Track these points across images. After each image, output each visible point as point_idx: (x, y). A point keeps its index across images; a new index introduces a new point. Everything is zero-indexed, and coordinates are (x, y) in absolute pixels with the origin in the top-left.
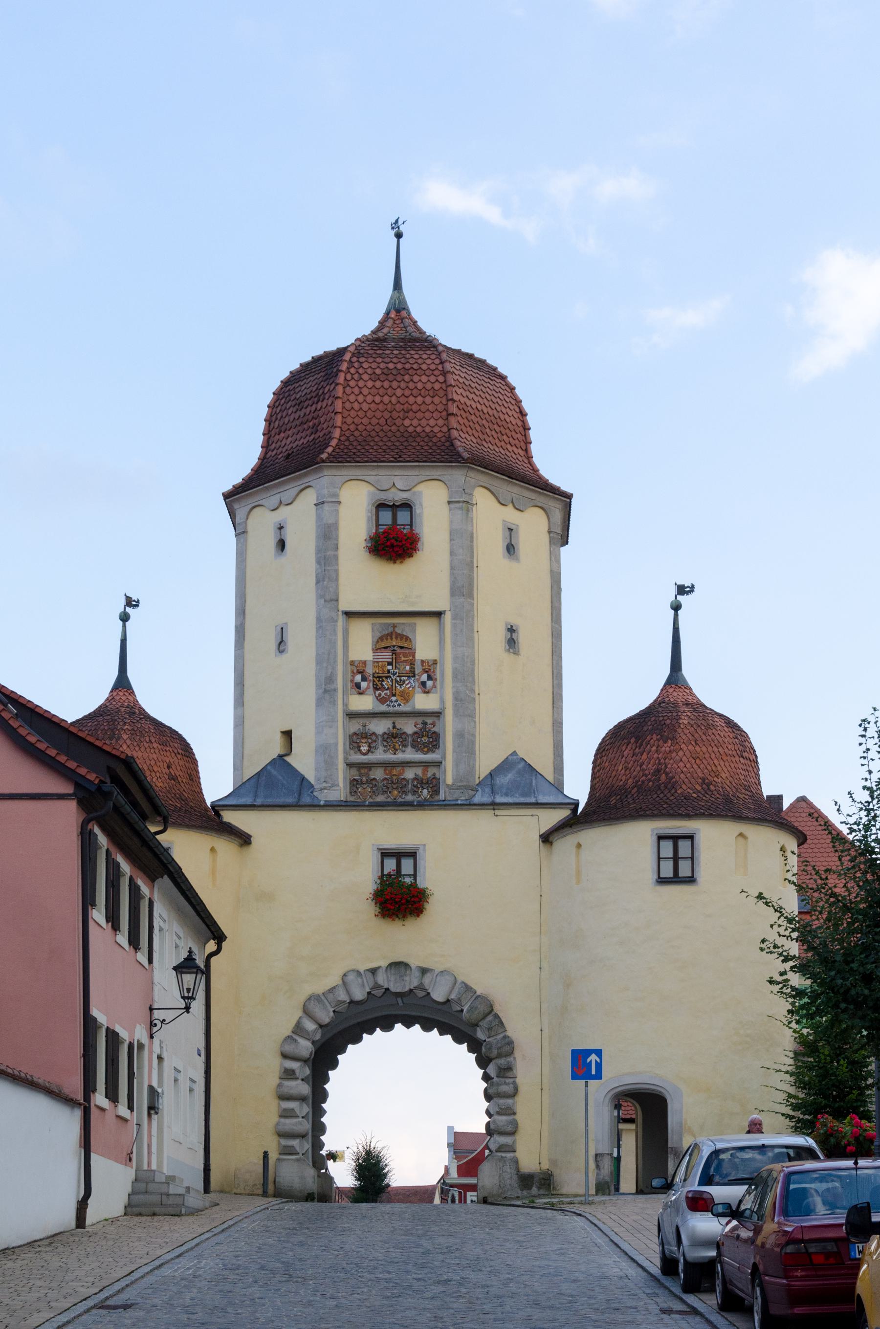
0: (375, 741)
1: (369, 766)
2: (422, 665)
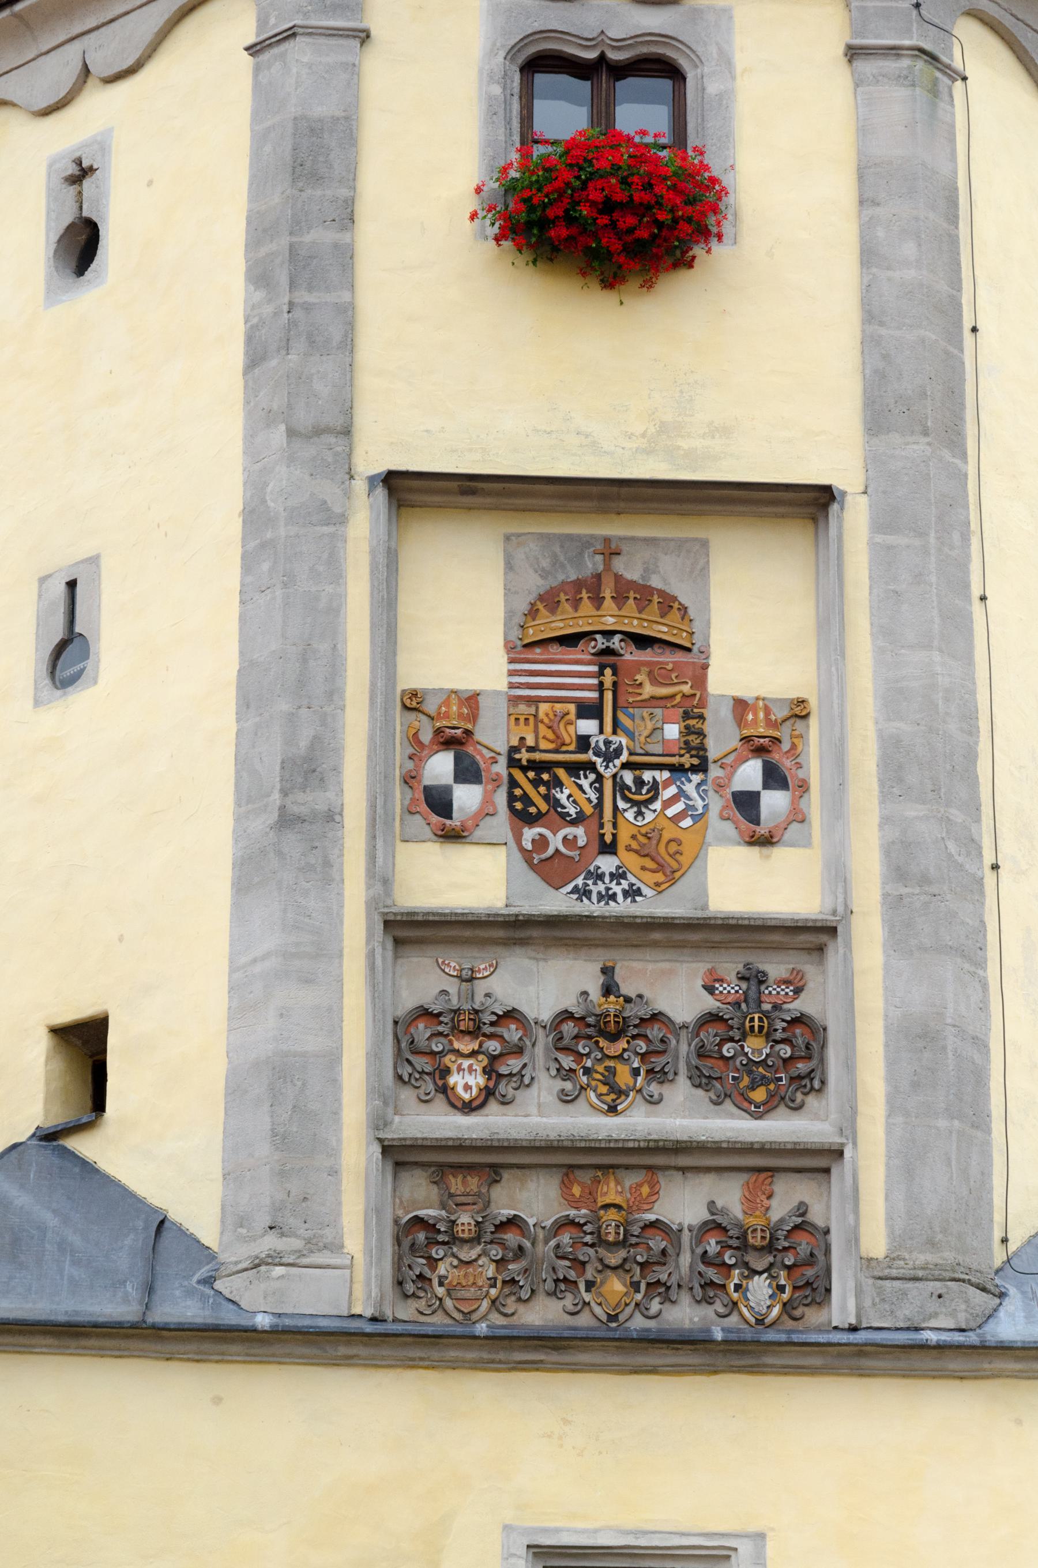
0: (519, 1050)
1: (492, 1162)
2: (739, 719)
